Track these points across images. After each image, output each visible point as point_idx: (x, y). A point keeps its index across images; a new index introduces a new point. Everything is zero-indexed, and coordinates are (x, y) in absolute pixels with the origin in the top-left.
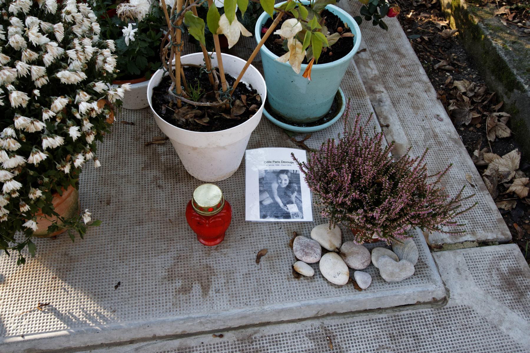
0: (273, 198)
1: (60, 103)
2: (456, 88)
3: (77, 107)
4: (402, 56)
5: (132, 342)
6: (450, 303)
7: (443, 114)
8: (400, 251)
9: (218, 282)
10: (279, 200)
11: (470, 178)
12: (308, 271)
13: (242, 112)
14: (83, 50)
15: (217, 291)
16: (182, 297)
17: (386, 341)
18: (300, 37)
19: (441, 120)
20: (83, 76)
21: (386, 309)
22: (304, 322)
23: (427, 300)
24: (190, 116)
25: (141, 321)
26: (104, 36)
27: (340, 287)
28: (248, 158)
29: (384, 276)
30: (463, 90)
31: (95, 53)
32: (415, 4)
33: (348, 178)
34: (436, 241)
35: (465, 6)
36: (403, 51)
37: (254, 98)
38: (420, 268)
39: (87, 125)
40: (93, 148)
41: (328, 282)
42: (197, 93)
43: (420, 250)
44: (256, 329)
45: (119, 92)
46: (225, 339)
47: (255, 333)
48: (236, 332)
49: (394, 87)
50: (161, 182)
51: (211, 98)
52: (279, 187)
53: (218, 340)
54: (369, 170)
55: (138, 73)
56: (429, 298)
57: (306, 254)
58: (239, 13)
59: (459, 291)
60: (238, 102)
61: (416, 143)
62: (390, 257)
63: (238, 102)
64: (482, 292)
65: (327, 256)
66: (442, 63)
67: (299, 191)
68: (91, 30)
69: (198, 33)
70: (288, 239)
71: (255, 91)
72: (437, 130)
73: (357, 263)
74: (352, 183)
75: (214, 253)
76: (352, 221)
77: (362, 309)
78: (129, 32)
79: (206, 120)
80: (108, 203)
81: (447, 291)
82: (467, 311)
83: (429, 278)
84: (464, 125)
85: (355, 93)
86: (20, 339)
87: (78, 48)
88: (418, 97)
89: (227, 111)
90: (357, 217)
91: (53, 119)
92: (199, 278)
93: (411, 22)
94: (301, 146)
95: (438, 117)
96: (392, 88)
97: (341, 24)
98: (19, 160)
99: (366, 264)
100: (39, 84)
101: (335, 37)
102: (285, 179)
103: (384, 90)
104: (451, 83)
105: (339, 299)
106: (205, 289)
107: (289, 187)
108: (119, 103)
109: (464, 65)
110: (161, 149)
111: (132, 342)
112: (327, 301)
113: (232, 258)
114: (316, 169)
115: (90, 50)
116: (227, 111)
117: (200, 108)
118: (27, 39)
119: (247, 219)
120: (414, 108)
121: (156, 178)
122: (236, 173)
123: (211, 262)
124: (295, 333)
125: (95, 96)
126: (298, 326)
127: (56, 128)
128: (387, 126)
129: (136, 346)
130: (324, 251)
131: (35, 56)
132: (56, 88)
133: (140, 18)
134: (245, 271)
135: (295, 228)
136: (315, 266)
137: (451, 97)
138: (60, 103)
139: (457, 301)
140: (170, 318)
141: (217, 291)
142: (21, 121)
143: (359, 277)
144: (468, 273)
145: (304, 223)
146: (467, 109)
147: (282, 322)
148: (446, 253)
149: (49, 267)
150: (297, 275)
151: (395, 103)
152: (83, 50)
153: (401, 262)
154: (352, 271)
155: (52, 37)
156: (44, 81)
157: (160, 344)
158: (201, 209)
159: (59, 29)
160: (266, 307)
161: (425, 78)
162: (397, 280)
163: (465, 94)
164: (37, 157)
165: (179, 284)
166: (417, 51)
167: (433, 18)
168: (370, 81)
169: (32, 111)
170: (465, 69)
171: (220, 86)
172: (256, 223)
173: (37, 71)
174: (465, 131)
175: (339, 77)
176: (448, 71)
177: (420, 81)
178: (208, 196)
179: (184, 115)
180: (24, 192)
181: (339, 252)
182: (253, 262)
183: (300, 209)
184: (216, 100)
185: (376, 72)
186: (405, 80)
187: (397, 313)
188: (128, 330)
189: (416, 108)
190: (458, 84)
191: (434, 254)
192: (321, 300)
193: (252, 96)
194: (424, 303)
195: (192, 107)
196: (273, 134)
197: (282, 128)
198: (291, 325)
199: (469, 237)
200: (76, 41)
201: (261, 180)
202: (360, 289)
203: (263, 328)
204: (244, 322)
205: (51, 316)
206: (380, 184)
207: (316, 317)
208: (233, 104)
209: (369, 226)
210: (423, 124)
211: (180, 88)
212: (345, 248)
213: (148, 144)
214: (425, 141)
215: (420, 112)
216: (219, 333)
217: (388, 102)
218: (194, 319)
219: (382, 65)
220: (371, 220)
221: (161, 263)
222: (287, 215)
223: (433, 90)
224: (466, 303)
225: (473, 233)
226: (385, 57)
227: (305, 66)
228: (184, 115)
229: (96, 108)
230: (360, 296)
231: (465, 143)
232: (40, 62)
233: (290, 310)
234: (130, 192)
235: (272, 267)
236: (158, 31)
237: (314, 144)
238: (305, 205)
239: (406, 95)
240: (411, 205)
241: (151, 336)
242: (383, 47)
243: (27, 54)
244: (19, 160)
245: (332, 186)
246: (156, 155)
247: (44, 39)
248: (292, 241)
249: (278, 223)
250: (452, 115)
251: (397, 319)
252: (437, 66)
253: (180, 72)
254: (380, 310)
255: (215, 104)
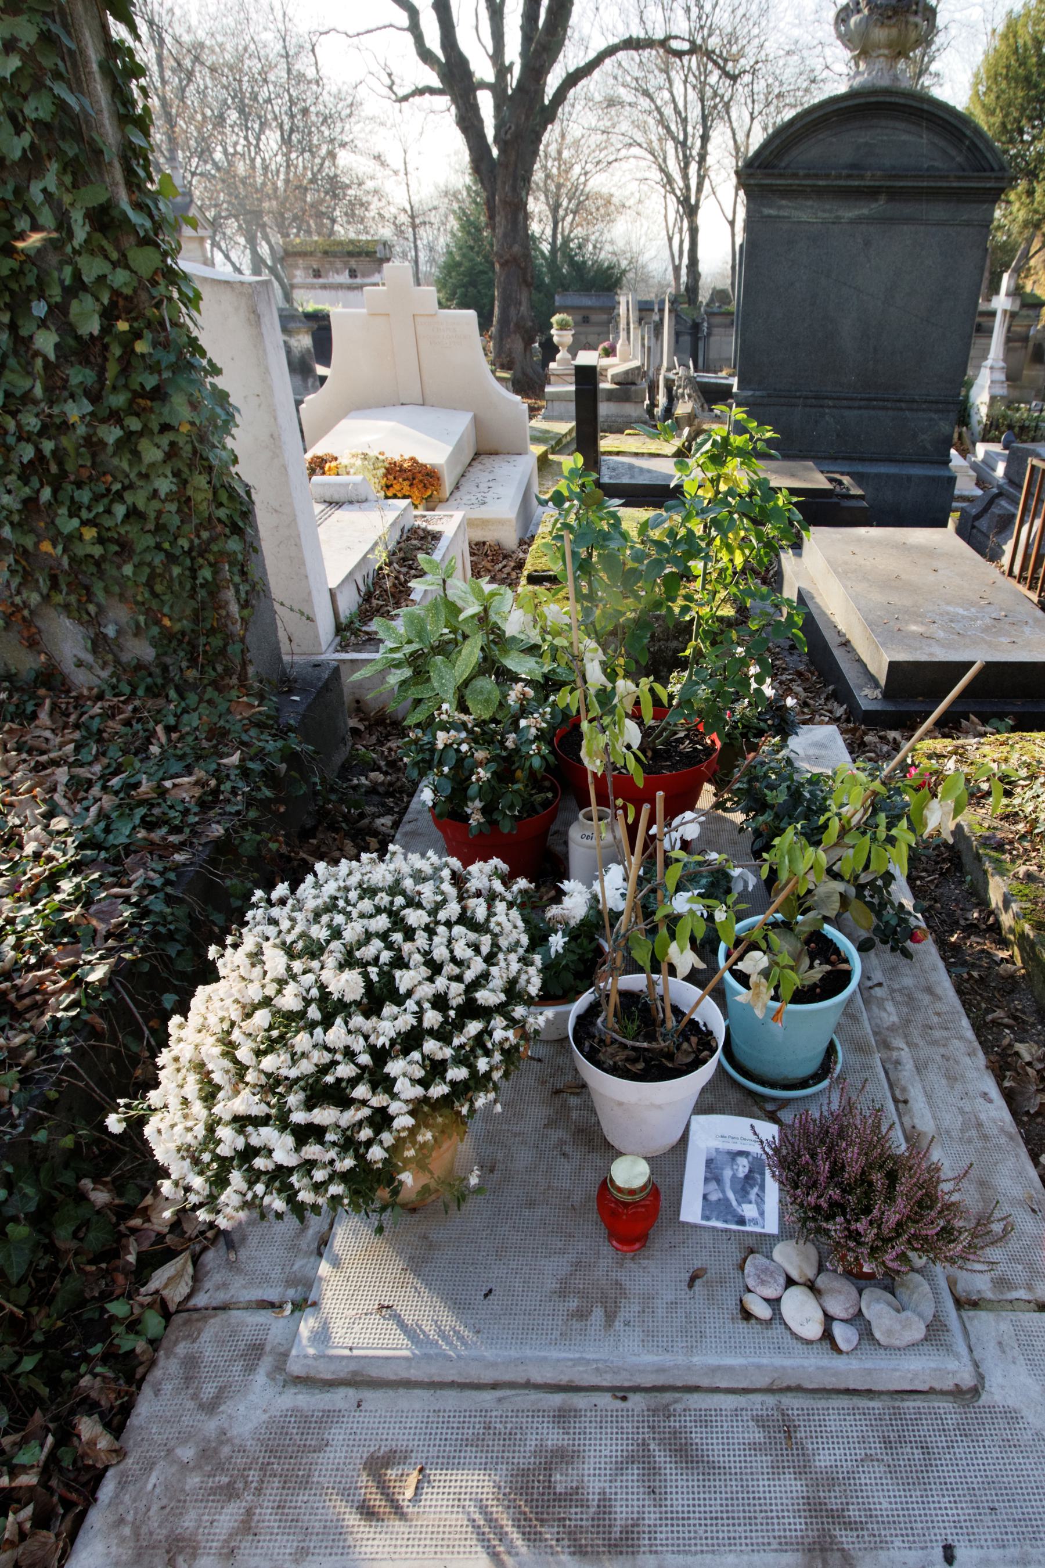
0: (723, 1192)
1: (474, 1027)
2: (1017, 1054)
3: (490, 1034)
4: (937, 998)
5: (495, 1386)
6: (984, 1399)
7: (994, 1093)
8: (905, 1298)
9: (629, 1310)
10: (731, 1195)
11: (1031, 1198)
12: (762, 1311)
13: (689, 1060)
14: (508, 966)
15: (627, 1324)
16: (576, 1325)
17: (877, 1449)
18: (766, 973)
19: (991, 1101)
20: (503, 997)
21: (881, 1393)
22: (750, 1396)
23: (946, 1388)
24: (620, 1057)
25: (513, 1353)
26: (531, 949)
27: (809, 1342)
28: (693, 1127)
29: (877, 1335)
30: (1028, 1058)
31: (519, 972)
32: (962, 922)
33: (825, 1167)
34: (968, 1293)
35: (1031, 934)
36: (939, 991)
37: (708, 1043)
38: (935, 1330)
39: (498, 1057)
40: (496, 1088)
41: (792, 1333)
42: (632, 1027)
43: (937, 1302)
44: (677, 1395)
45: (541, 1018)
46: (628, 1404)
47: (676, 1402)
48: (647, 1396)
49: (921, 1043)
50: (567, 1149)
51: (651, 1037)
52: (734, 1177)
53: (619, 1404)
54: (852, 1156)
55: (560, 993)
56: (948, 1385)
57: (763, 1282)
58: (693, 940)
59: (1000, 1380)
60: (685, 1045)
61: (948, 1132)
62: (889, 1304)
63: (685, 1045)
64: (1038, 1388)
65: (793, 1290)
66: (999, 1014)
67: (762, 1187)
68: (518, 943)
69: (642, 956)
70: (738, 1256)
71: (710, 1033)
72: (983, 1117)
73: (838, 1307)
74: (831, 1177)
75: (629, 1264)
76: (827, 1232)
77: (842, 1386)
78: (557, 942)
79: (641, 1065)
80: (492, 1171)
81: (981, 1377)
82: (1012, 1416)
83: (949, 1349)
84: (1027, 1113)
85: (860, 1047)
86: (347, 1352)
87: (503, 964)
88: (957, 1062)
89: (670, 1056)
90: (835, 1227)
91: (462, 1046)
92: (604, 1300)
93: (956, 948)
94: (772, 1117)
95: (985, 1095)
96: (916, 1045)
97: (837, 951)
98: (418, 1091)
99: (851, 1311)
100: (454, 1003)
101: (820, 970)
102: (743, 1166)
103: (903, 1046)
104: (1010, 1046)
105: (806, 1363)
106: (610, 1318)
107: (747, 1177)
108: (536, 1032)
109: (1032, 1020)
110: (574, 1101)
111: (495, 1386)
112: (788, 1362)
113: (655, 1275)
114: (784, 1152)
115: (515, 967)
116: (670, 1056)
117: (634, 1048)
118: (452, 952)
119: (683, 1217)
120: (948, 1078)
121: (562, 1142)
122: (674, 1148)
123: (622, 1276)
124: (736, 1412)
125: (512, 1022)
126: (741, 1401)
127: (464, 1059)
128: (906, 1102)
129: (499, 1393)
130: (790, 1282)
131: (457, 971)
132: (471, 1010)
133: (573, 923)
134: (670, 1298)
135: (750, 1242)
136: (774, 1303)
137: (1008, 1066)
138: (474, 1027)
139: (997, 1398)
140: (555, 1354)
141: (627, 1324)
142: (430, 1046)
143: (839, 1331)
144: (1016, 1352)
145: (765, 1235)
146: (1033, 1088)
147: (717, 1390)
148: (983, 1314)
149: (399, 1253)
150: (747, 1315)
151: (920, 1068)
152: (508, 966)
153: (904, 1314)
154: (829, 1319)
155: (476, 948)
156: (460, 1000)
157: (534, 1396)
158: (620, 1190)
159: (486, 941)
160: (695, 1359)
161: (970, 1034)
162: (897, 1343)
163: (1029, 1064)
164: (438, 1090)
165: (573, 1304)
166: (959, 992)
167: (988, 946)
168: (885, 1032)
169: (443, 1035)
170: (1033, 1025)
171: (664, 1021)
172: (695, 1227)
173: (457, 988)
174: (1029, 1123)
175: (833, 1019)
176: (1008, 1026)
177: (961, 1038)
178: (630, 1173)
179: (613, 1056)
180: (413, 1131)
181: (811, 1286)
182: (684, 1285)
183: (762, 1213)
184: (656, 1040)
185: (894, 1018)
186: (938, 1034)
187: (897, 1404)
188: (494, 1365)
189: (952, 1078)
190: (1019, 1047)
191: (964, 1314)
192: (779, 1361)
193: (704, 1039)
194: (943, 1393)
195: (625, 1047)
196: (734, 1096)
197: (744, 1087)
198: (731, 1398)
199: (1022, 1294)
200: (501, 956)
201: (709, 1162)
202: (839, 1351)
203: (687, 1396)
204: (661, 1380)
205: (392, 1325)
206: (871, 1184)
207: (769, 1390)
208: (678, 1047)
209: (852, 1244)
210: (961, 1104)
211: (612, 1020)
212: (821, 1282)
213: (557, 1092)
214: (962, 1131)
215: (958, 1086)
216: (621, 1393)
217: (909, 1065)
218: (588, 1362)
219: (905, 1010)
220: (855, 1236)
221: (553, 1268)
222: (742, 1221)
223: (980, 1054)
224: (1010, 1403)
225: (1030, 1288)
226: (911, 998)
227: (777, 1005)
228: (613, 1056)
229: (512, 1037)
230: (839, 1363)
231: (1027, 1142)
232: (459, 979)
233: (730, 1370)
234: (523, 1157)
235: (710, 1297)
236: (592, 939)
237: (787, 1116)
238: (768, 1209)
239: (938, 1058)
240: (915, 1217)
241: (522, 1381)
242: (908, 982)
243: (450, 969)
244: (418, 1091)
245: (804, 1179)
246: (565, 1107)
247: (469, 953)
248: (745, 1260)
249: (726, 1230)
250: (1009, 1096)
251: (897, 1413)
252: (990, 1017)
253: (614, 998)
254: (869, 1393)
255: (654, 1045)
